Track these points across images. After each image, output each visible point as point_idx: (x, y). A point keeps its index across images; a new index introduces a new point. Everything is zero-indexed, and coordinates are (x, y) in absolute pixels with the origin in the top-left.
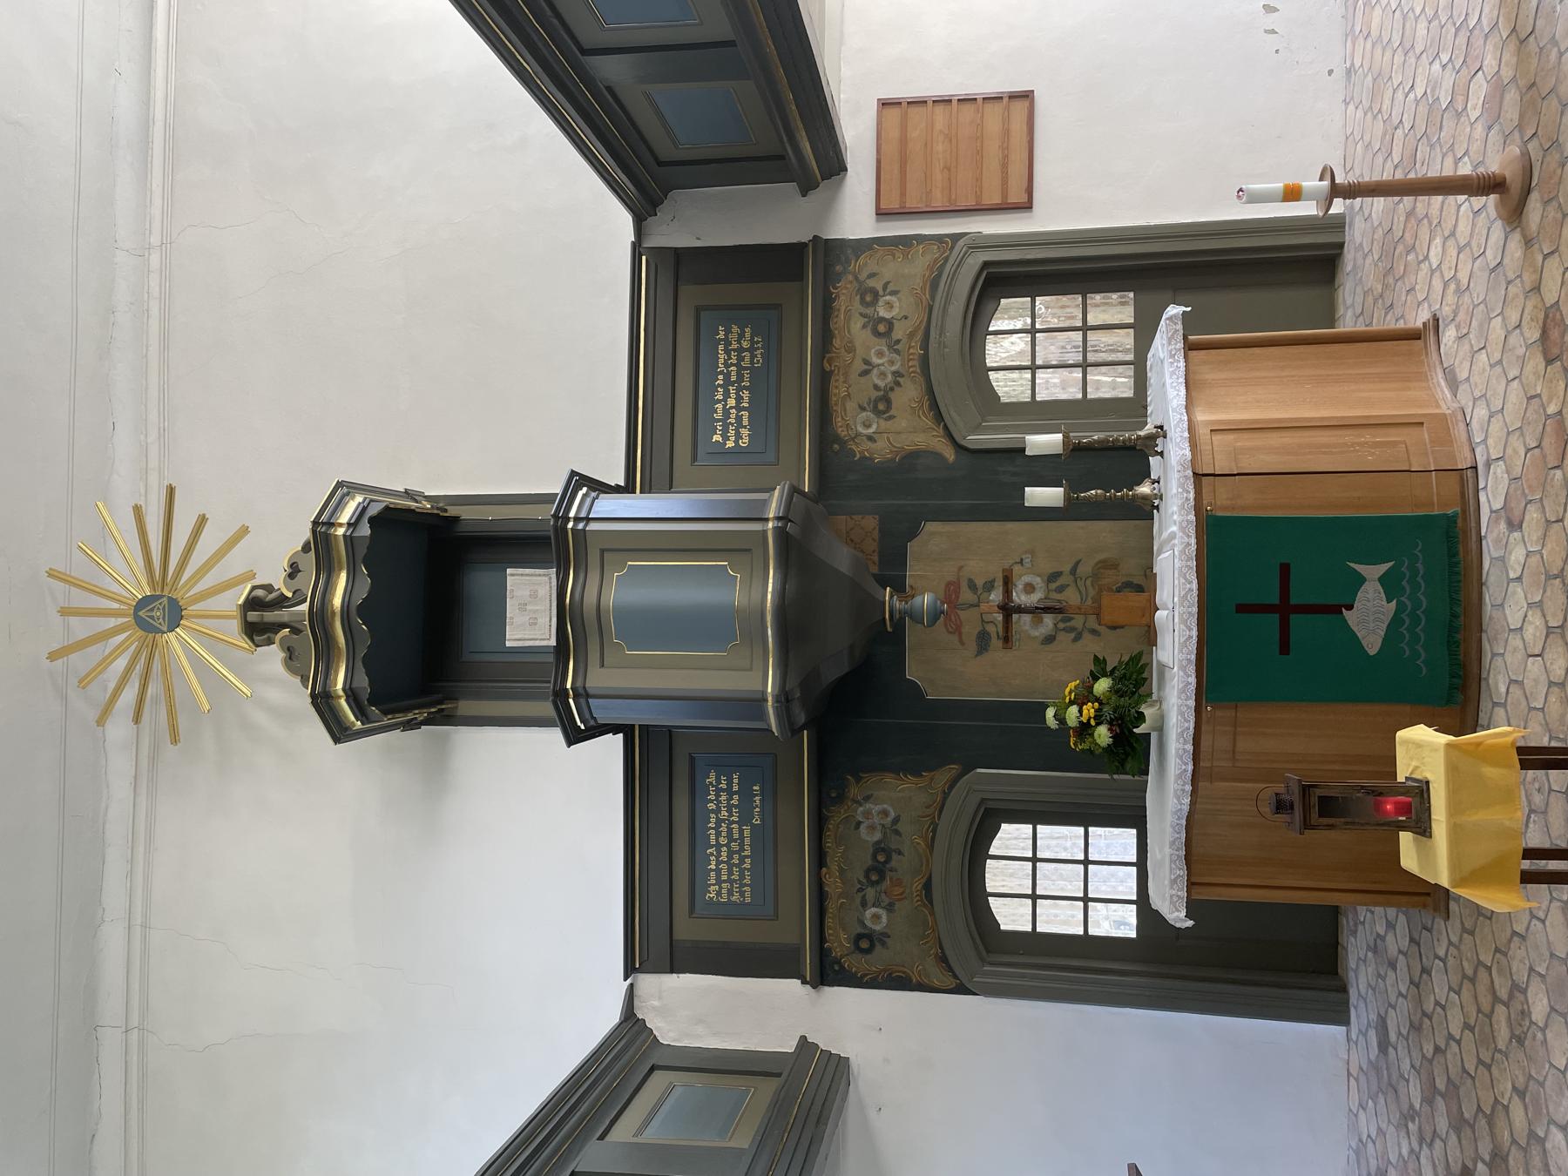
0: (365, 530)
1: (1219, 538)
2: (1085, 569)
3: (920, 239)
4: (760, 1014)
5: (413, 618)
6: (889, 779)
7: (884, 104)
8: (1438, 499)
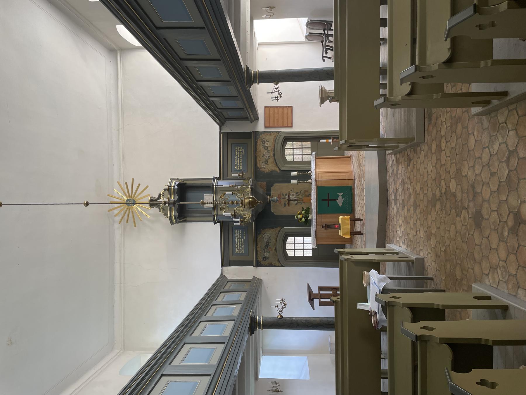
0: (176, 187)
1: (318, 188)
2: (302, 192)
3: (273, 132)
4: (247, 272)
5: (184, 202)
6: (269, 230)
7: (265, 107)
8: (350, 184)
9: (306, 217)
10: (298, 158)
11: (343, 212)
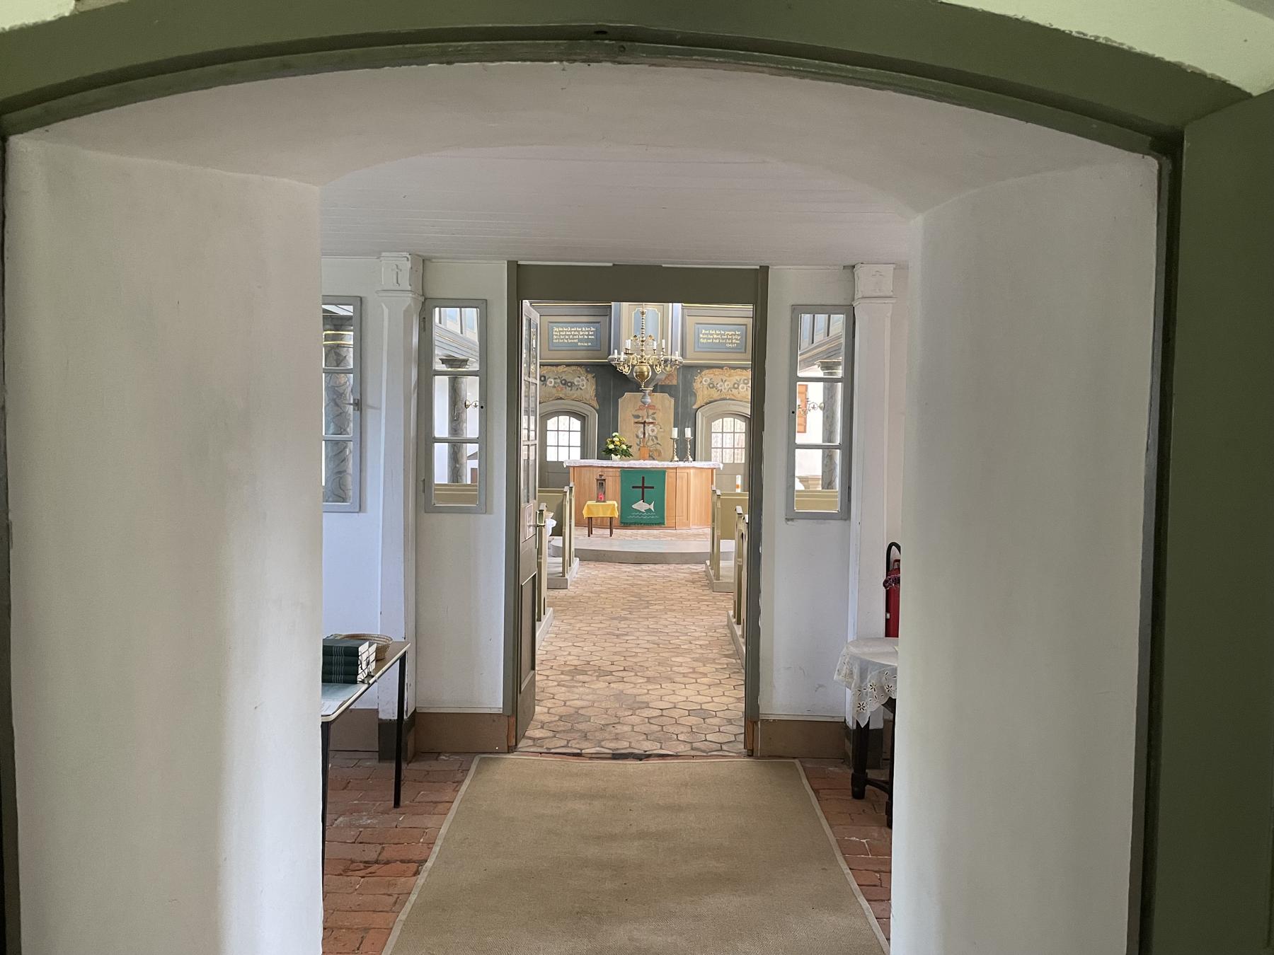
1: (661, 473)
9: (615, 451)
10: (716, 440)
11: (625, 506)
